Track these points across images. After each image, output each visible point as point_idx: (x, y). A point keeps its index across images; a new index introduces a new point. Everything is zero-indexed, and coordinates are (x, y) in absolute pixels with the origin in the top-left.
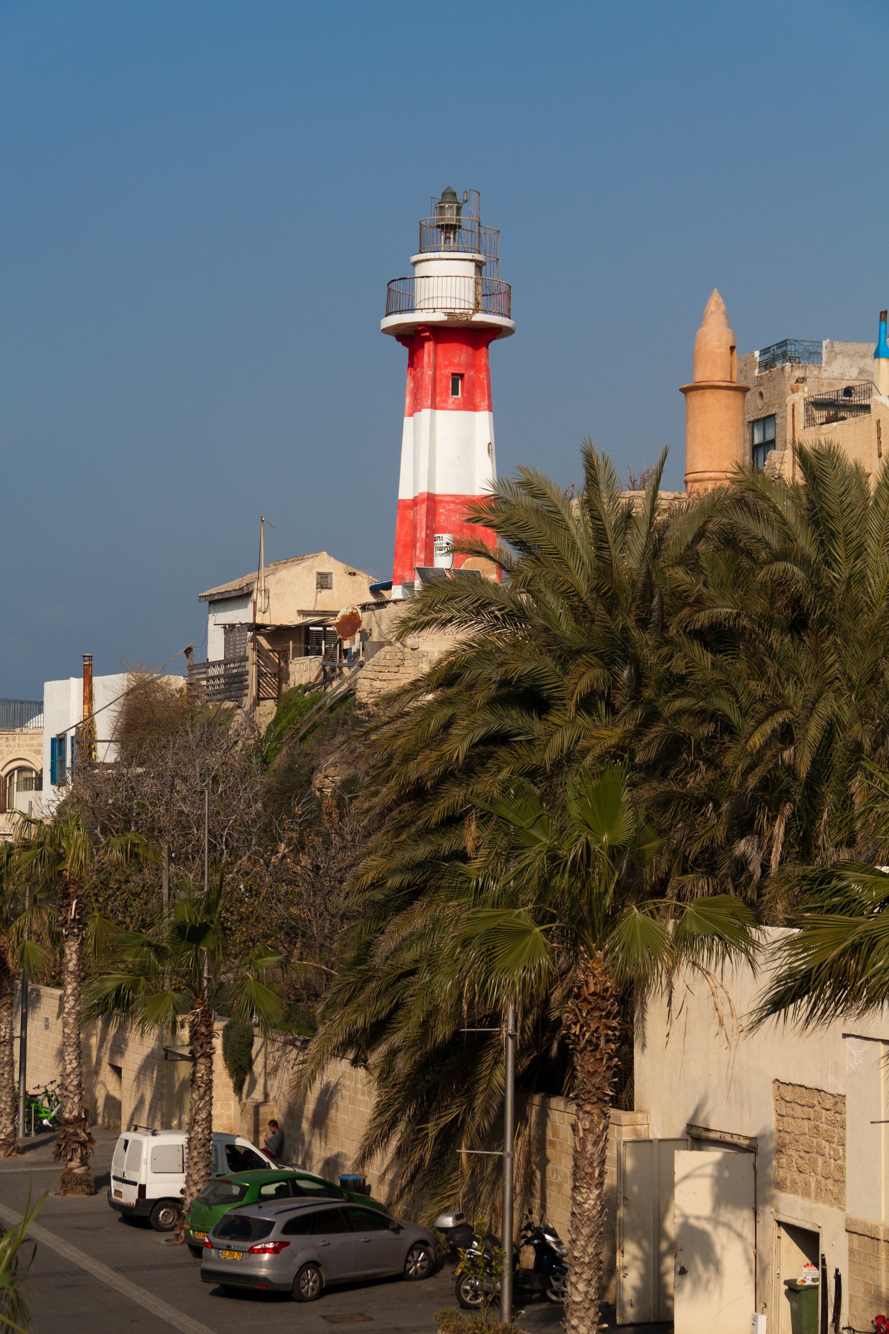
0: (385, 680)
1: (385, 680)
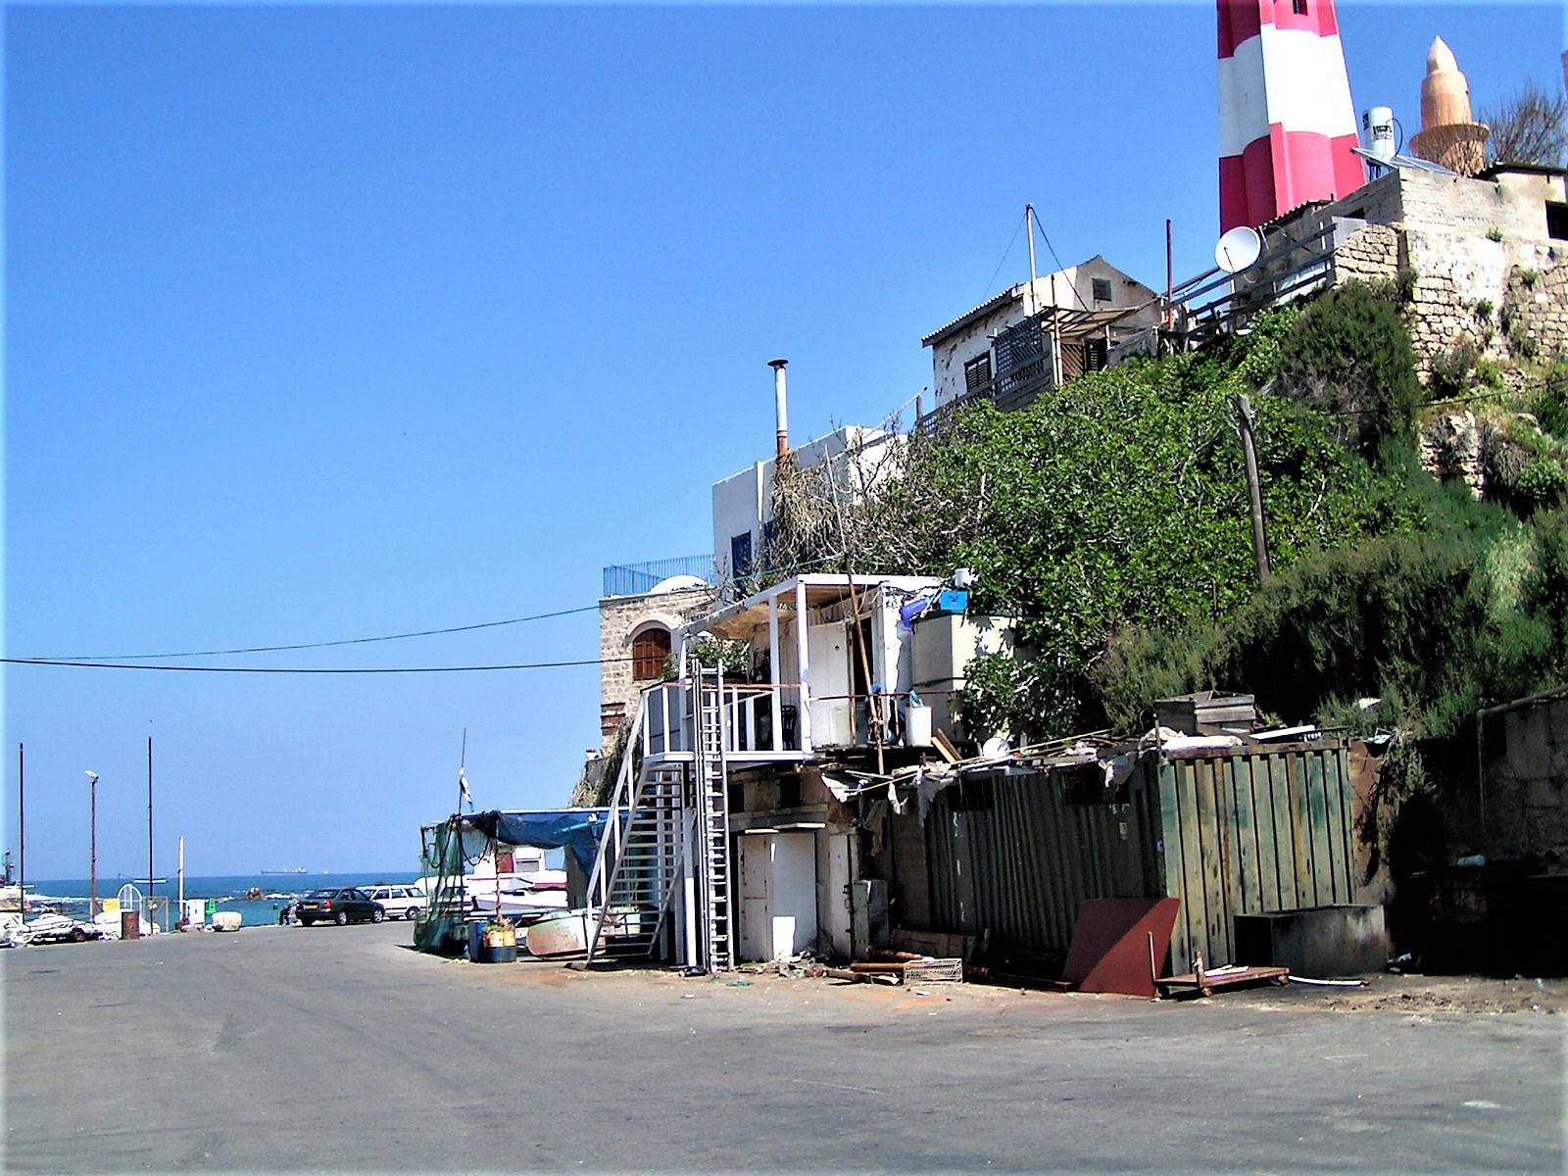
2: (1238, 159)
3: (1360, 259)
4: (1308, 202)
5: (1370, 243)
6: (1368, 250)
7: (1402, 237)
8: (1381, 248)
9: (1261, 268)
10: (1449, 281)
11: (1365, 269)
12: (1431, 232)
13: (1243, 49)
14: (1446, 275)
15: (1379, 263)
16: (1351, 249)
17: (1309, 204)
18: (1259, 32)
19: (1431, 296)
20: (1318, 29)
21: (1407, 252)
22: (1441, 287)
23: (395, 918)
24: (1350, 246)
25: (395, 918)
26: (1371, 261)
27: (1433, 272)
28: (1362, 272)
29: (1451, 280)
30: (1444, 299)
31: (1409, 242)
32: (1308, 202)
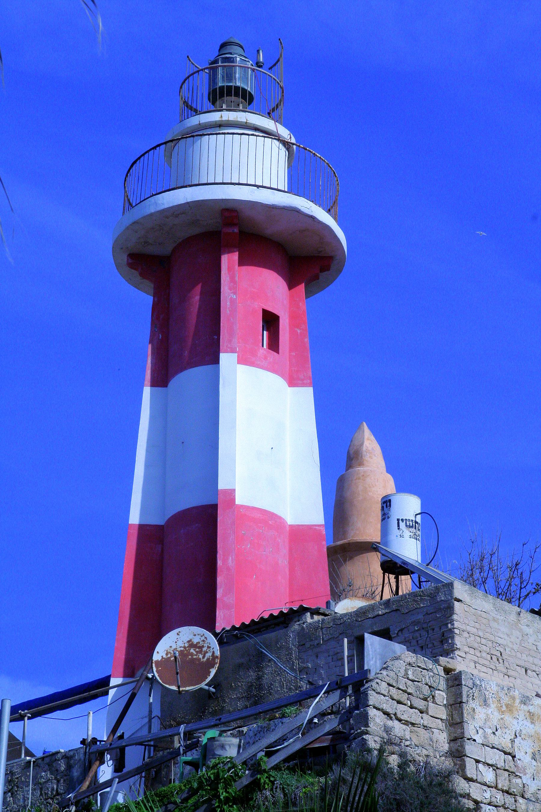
0: (407, 723)
1: (407, 723)
2: (159, 528)
3: (399, 702)
4: (301, 606)
5: (413, 681)
6: (409, 691)
7: (454, 680)
8: (426, 690)
9: (317, 656)
10: (510, 757)
11: (404, 717)
12: (493, 682)
13: (188, 379)
14: (506, 744)
15: (422, 712)
16: (389, 685)
17: (303, 610)
18: (216, 361)
19: (489, 776)
20: (142, 523)
21: (461, 702)
22: (501, 764)
23: (198, 635)
24: (388, 679)
25: (198, 635)
26: (412, 707)
27: (494, 740)
28: (400, 720)
29: (514, 757)
30: (503, 783)
31: (465, 690)
32: (301, 606)
